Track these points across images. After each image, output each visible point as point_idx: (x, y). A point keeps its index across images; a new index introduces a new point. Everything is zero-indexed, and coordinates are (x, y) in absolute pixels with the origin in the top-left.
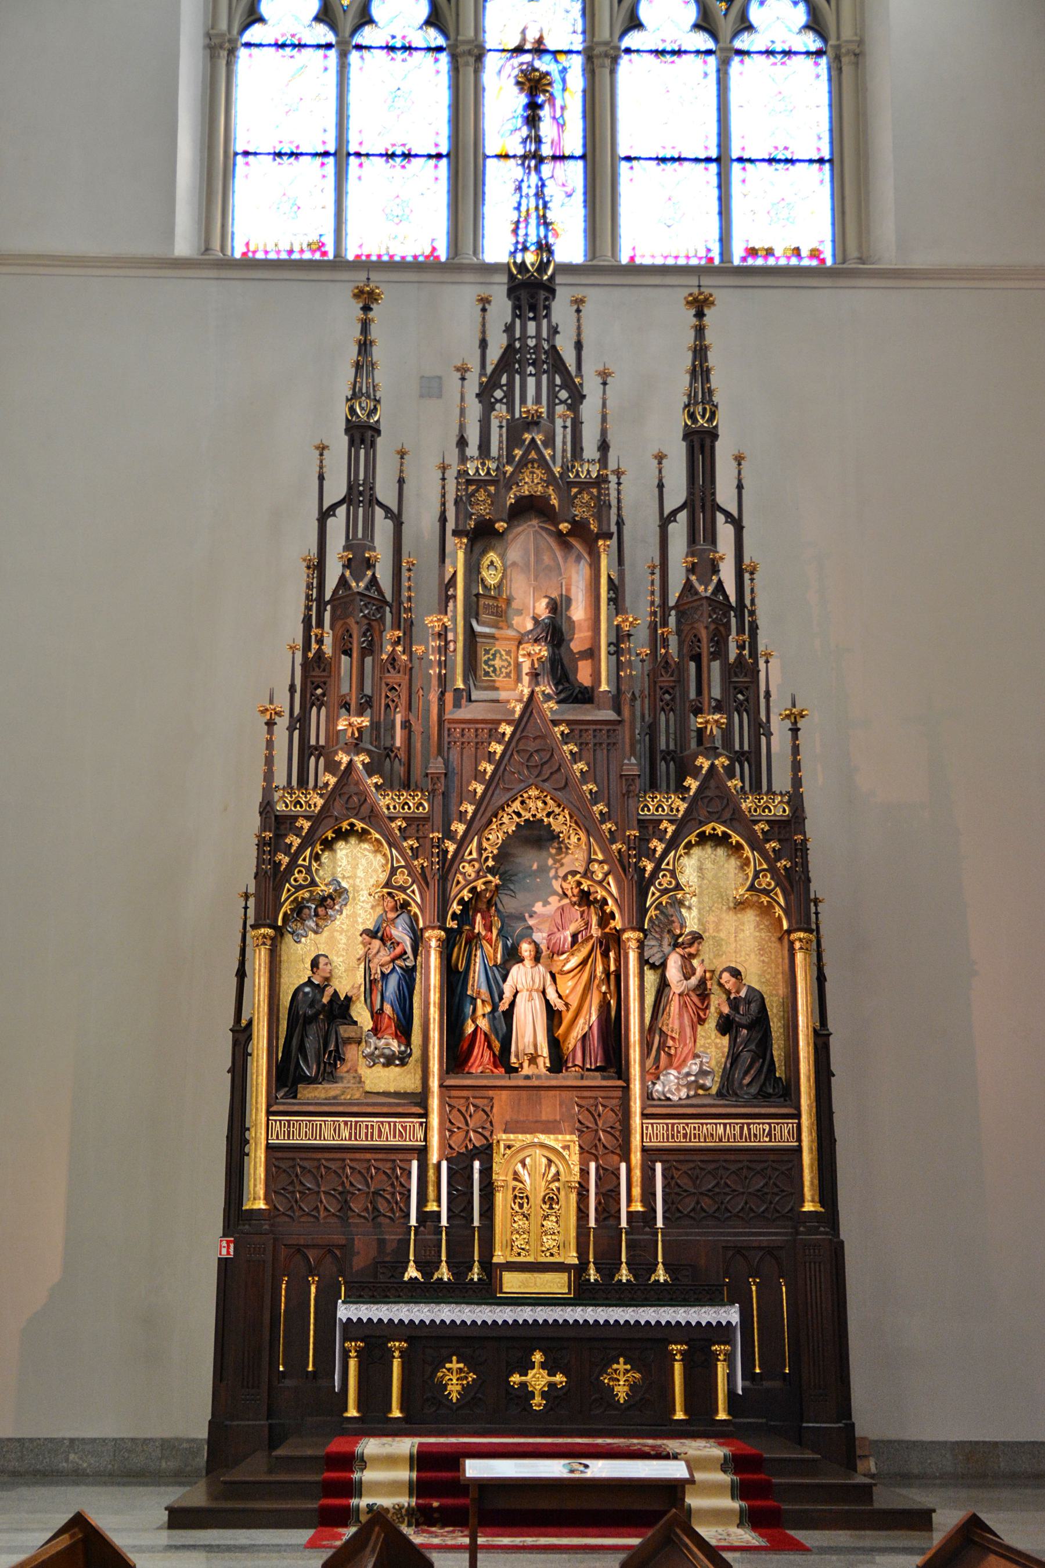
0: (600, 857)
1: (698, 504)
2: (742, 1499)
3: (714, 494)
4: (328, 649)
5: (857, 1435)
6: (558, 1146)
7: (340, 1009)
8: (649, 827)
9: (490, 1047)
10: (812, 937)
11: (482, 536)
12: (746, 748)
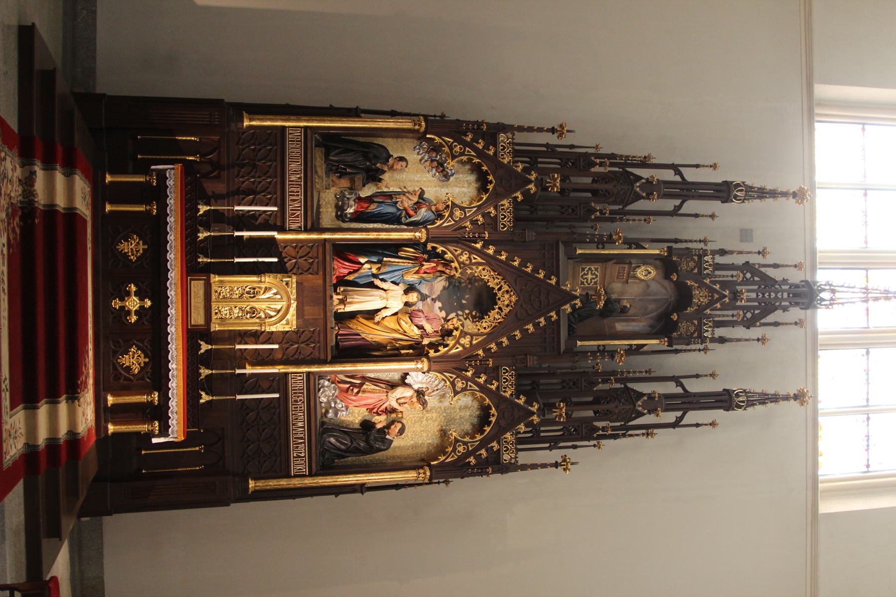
0: (474, 342)
1: (686, 400)
2: (47, 446)
3: (694, 409)
4: (597, 169)
5: (106, 520)
6: (289, 317)
7: (374, 176)
8: (494, 374)
9: (350, 273)
10: (427, 481)
11: (667, 265)
12: (542, 434)
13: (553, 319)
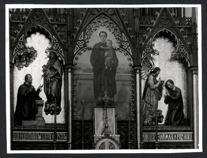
13: (52, 19)
